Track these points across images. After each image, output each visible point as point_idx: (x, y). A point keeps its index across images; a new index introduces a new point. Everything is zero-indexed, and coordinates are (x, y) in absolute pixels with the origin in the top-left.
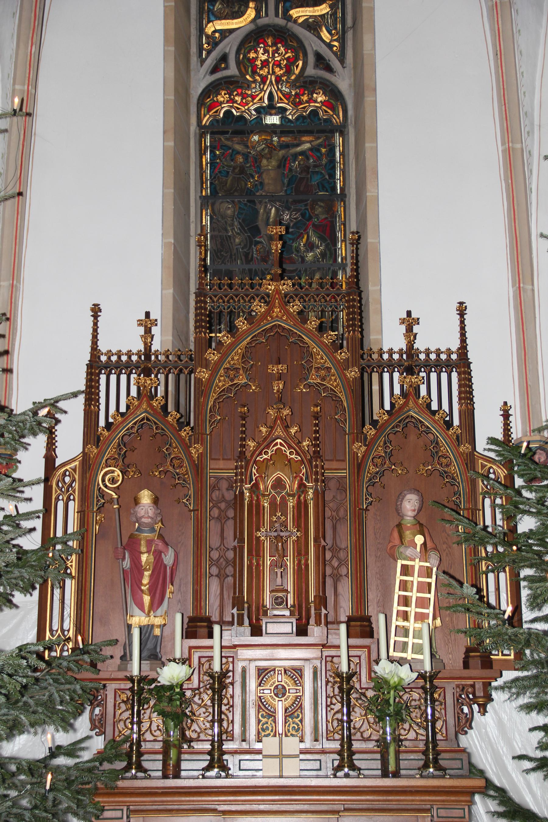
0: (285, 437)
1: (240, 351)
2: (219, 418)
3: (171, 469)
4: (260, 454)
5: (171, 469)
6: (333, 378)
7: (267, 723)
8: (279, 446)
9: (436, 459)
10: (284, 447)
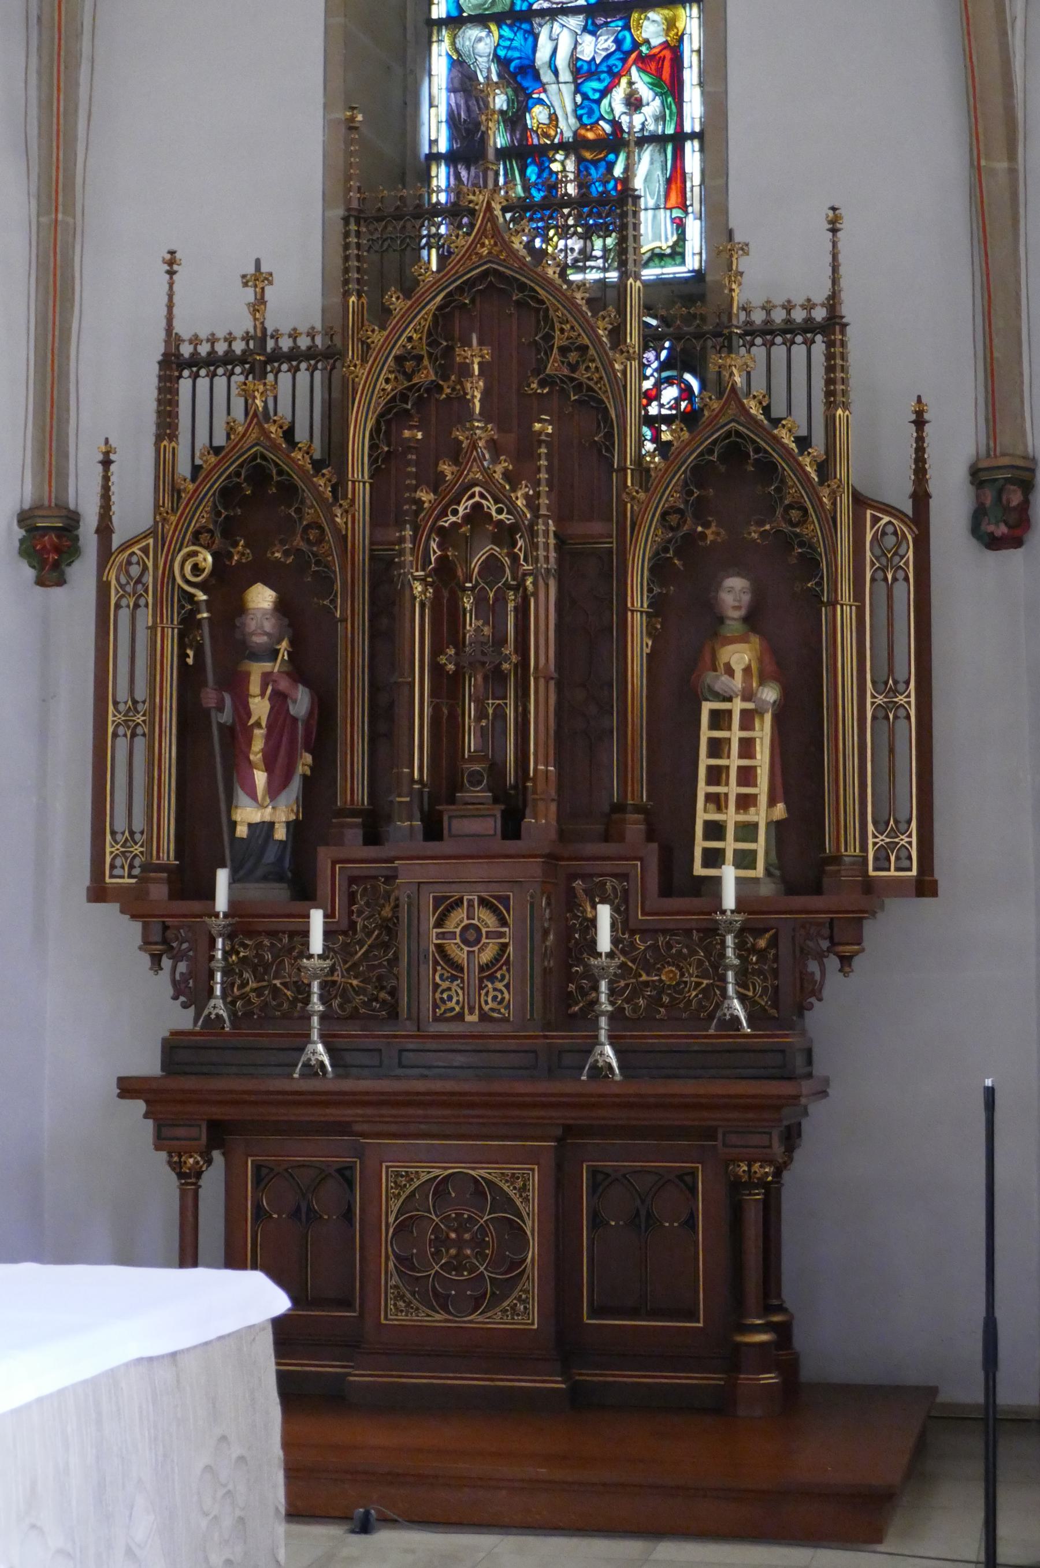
0: (486, 482)
1: (423, 323)
2: (386, 449)
3: (303, 546)
4: (444, 514)
5: (303, 546)
6: (592, 365)
7: (449, 989)
8: (477, 498)
9: (779, 511)
10: (487, 500)
